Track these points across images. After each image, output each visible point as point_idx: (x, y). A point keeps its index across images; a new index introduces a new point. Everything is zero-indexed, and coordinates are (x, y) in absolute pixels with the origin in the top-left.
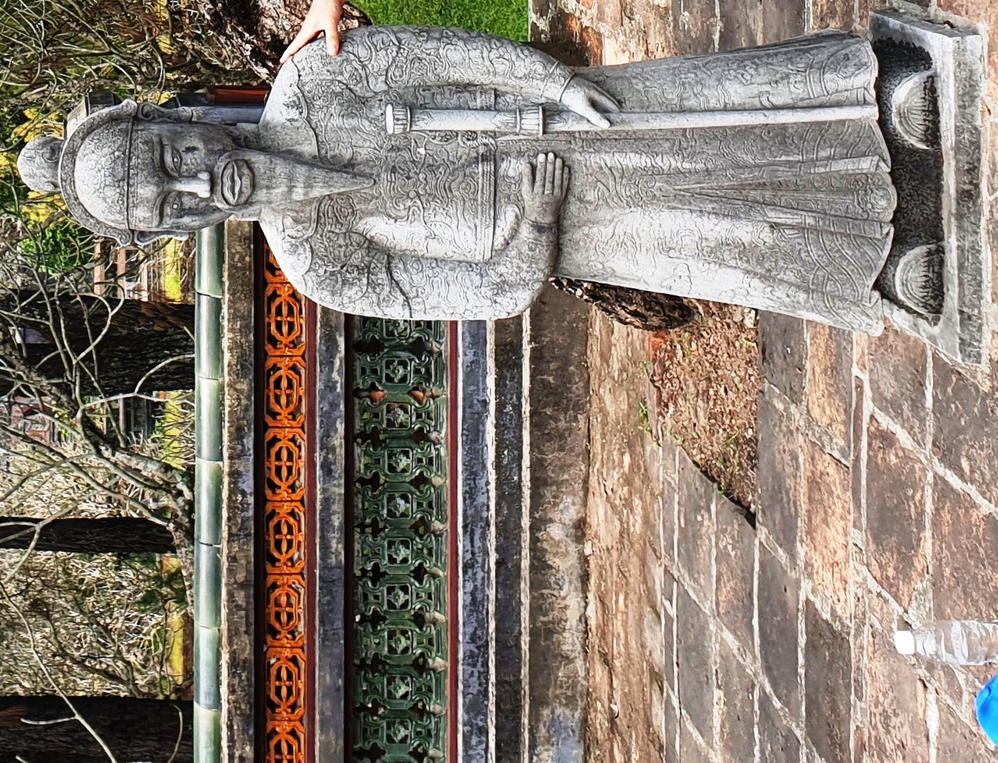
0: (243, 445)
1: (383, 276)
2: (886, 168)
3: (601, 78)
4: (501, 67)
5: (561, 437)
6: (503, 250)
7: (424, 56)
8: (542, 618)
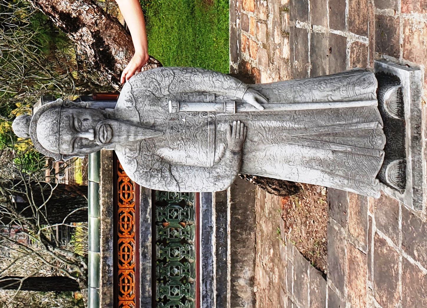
0: (109, 246)
1: (167, 174)
2: (381, 127)
3: (260, 89)
4: (218, 84)
5: (244, 242)
6: (219, 162)
7: (185, 79)
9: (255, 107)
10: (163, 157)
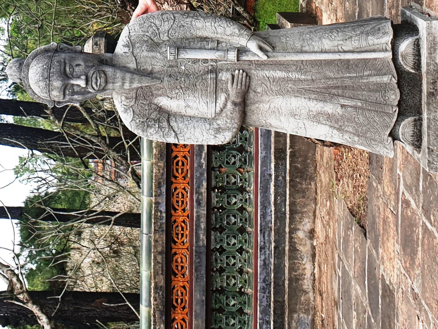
0: (161, 191)
1: (165, 124)
2: (395, 81)
4: (220, 30)
5: (304, 192)
6: (220, 113)
7: (185, 24)
8: (294, 273)
9: (258, 56)
10: (161, 106)
